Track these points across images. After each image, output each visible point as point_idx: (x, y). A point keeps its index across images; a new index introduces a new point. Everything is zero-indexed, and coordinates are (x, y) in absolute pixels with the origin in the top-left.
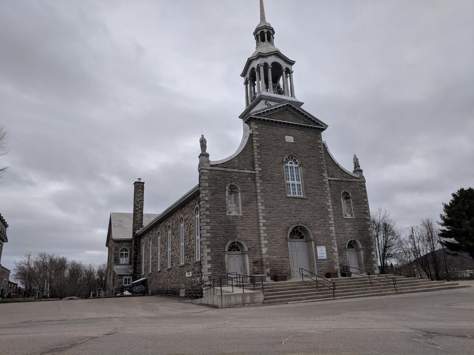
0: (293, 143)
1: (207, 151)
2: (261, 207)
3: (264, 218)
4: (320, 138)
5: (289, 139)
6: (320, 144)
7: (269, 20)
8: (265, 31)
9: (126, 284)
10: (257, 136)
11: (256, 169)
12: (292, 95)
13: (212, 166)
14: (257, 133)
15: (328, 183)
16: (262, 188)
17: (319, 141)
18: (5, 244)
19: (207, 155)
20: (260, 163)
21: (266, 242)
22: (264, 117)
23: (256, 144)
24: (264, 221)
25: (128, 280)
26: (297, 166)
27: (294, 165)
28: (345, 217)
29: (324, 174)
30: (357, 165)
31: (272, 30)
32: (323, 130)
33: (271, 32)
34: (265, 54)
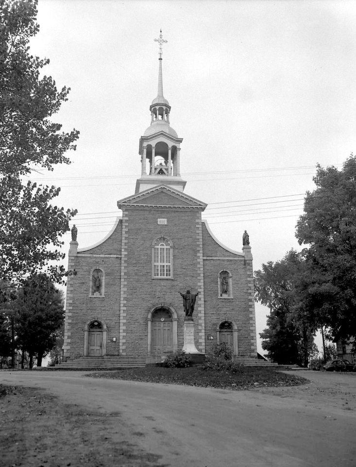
0: (166, 225)
1: (78, 240)
2: (123, 289)
3: (125, 299)
4: (200, 218)
5: (162, 221)
6: (198, 223)
7: (167, 96)
8: (164, 108)
9: (164, 276)
10: (126, 221)
11: (123, 253)
12: (176, 174)
13: (78, 253)
14: (127, 218)
15: (202, 263)
16: (126, 271)
17: (197, 221)
18: (205, 216)
19: (77, 244)
20: (126, 247)
21: (125, 321)
22: (133, 203)
23: (124, 230)
24: (125, 302)
25: (165, 271)
26: (168, 247)
27: (165, 247)
28: (221, 297)
29: (198, 255)
30: (246, 241)
31: (170, 108)
32: (203, 209)
33: (169, 109)
34: (148, 137)
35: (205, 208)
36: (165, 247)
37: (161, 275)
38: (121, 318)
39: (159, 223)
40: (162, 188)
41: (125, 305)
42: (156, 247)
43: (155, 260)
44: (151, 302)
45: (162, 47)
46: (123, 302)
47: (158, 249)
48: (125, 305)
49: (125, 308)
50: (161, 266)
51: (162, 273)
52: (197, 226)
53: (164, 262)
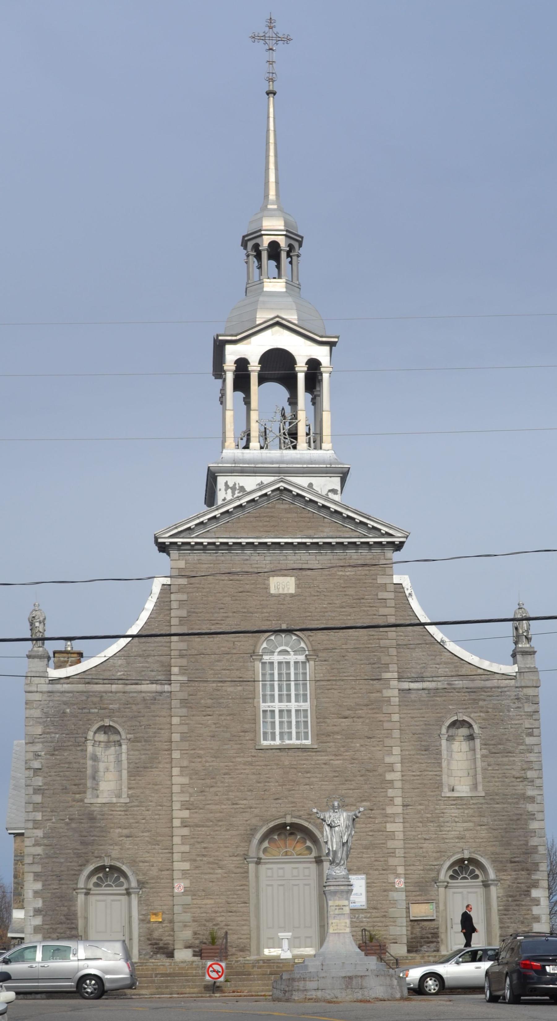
2: (179, 780)
6: (384, 587)
26: (301, 658)
27: (292, 658)
35: (402, 543)
36: (292, 658)
37: (298, 738)
38: (176, 857)
39: (273, 591)
40: (278, 489)
41: (184, 824)
42: (266, 658)
43: (264, 696)
44: (257, 811)
45: (274, 56)
46: (180, 814)
47: (272, 663)
48: (184, 824)
49: (186, 831)
50: (281, 711)
51: (302, 729)
52: (382, 595)
53: (289, 701)
